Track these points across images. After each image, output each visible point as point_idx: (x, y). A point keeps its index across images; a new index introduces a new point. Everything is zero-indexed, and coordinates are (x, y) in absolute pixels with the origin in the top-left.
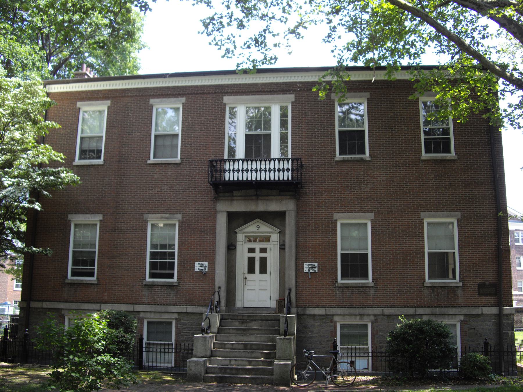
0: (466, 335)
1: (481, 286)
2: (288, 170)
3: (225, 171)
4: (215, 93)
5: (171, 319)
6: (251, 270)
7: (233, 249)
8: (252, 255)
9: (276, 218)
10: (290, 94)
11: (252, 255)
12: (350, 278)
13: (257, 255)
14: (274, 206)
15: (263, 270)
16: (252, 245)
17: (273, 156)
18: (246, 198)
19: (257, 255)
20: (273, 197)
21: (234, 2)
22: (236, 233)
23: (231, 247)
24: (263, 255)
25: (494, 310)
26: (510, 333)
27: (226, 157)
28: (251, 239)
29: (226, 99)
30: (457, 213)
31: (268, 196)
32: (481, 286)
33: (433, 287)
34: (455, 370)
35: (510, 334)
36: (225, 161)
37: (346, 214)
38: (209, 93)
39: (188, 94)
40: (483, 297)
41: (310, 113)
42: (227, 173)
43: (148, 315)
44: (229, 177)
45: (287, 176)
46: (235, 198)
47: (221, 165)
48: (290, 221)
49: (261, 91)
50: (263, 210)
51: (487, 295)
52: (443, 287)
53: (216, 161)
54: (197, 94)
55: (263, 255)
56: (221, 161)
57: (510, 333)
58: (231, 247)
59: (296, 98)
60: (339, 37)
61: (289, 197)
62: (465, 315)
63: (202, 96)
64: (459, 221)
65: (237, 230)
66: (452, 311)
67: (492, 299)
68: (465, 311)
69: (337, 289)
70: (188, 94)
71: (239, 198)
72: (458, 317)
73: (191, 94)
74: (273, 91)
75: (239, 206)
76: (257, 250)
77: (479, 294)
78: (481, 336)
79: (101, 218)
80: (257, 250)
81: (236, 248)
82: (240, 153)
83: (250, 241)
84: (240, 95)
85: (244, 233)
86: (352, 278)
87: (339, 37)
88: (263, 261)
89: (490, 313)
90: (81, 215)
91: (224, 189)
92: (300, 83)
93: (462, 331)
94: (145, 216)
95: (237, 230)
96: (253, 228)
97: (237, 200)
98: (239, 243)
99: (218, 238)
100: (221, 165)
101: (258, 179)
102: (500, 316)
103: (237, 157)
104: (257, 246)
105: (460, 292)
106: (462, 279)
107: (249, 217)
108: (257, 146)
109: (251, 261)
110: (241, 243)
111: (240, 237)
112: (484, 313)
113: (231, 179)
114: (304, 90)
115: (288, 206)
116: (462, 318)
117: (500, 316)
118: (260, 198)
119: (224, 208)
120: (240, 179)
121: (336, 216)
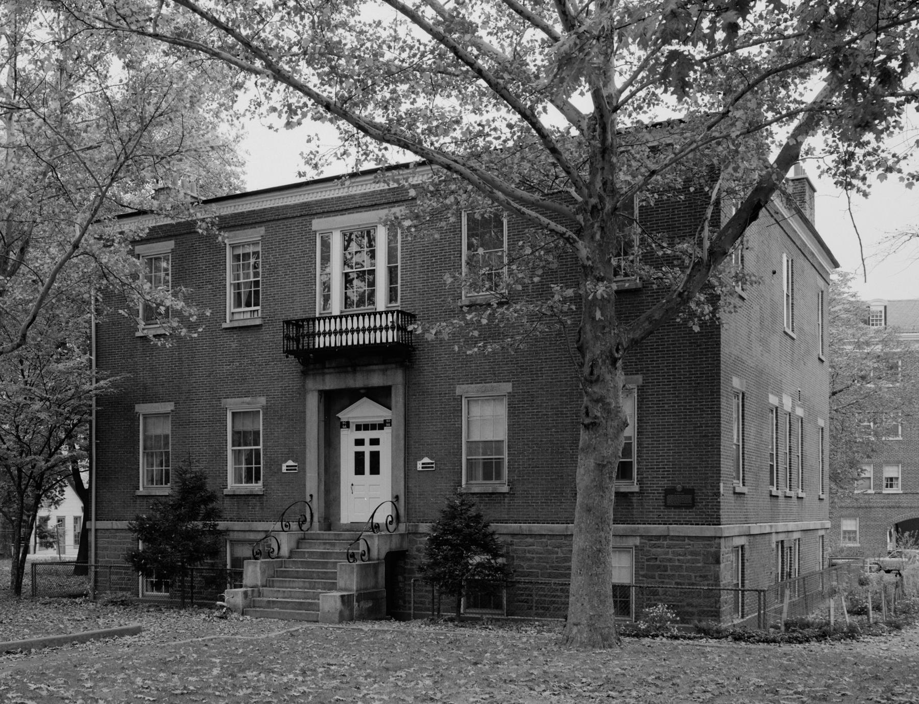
1: (669, 491)
2: (319, 334)
4: (301, 216)
6: (359, 470)
8: (360, 449)
9: (381, 396)
11: (360, 449)
13: (367, 449)
14: (376, 380)
15: (375, 470)
16: (361, 435)
18: (342, 370)
19: (367, 449)
20: (375, 367)
21: (1, 298)
24: (375, 448)
29: (318, 224)
30: (636, 376)
31: (366, 365)
37: (473, 386)
38: (293, 217)
44: (321, 342)
45: (391, 336)
46: (326, 371)
48: (398, 398)
50: (381, 385)
53: (303, 320)
54: (278, 220)
55: (375, 448)
56: (308, 320)
61: (394, 366)
63: (285, 221)
71: (331, 370)
75: (331, 383)
76: (367, 442)
77: (667, 506)
80: (367, 442)
82: (336, 307)
88: (375, 456)
91: (314, 360)
94: (223, 401)
97: (330, 373)
99: (308, 427)
101: (355, 343)
103: (333, 314)
104: (367, 435)
107: (352, 396)
109: (359, 457)
113: (367, 342)
115: (396, 379)
116: (637, 541)
118: (358, 368)
119: (315, 385)
120: (327, 344)
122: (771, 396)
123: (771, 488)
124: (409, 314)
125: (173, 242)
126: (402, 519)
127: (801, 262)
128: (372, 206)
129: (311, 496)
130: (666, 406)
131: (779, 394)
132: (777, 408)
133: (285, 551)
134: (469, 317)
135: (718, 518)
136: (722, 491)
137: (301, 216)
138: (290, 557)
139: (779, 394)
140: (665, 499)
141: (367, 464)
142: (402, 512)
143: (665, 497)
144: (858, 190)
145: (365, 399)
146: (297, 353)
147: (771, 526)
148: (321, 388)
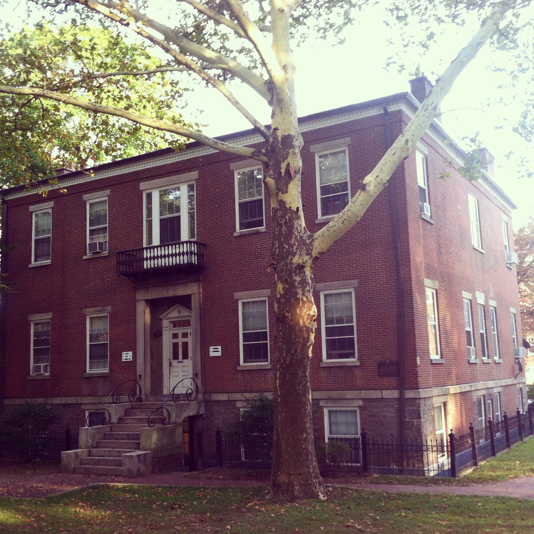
0: (366, 424)
1: (381, 365)
3: (143, 259)
4: (133, 181)
5: (103, 409)
6: (175, 356)
7: (159, 336)
8: (176, 341)
10: (194, 171)
11: (176, 341)
12: (253, 360)
13: (180, 340)
15: (185, 356)
17: (182, 240)
22: (161, 320)
23: (156, 334)
25: (394, 394)
26: (415, 422)
27: (145, 246)
28: (175, 324)
29: (143, 186)
30: (353, 281)
32: (381, 365)
33: (329, 368)
34: (358, 465)
35: (415, 423)
36: (143, 249)
38: (128, 182)
39: (111, 185)
40: (385, 378)
41: (212, 189)
42: (145, 262)
43: (88, 407)
44: (147, 265)
47: (140, 254)
49: (169, 173)
51: (388, 376)
52: (341, 367)
53: (136, 250)
54: (118, 184)
57: (415, 422)
58: (157, 334)
59: (199, 175)
60: (444, 63)
62: (364, 400)
64: (356, 289)
65: (161, 317)
66: (349, 394)
67: (393, 380)
68: (364, 394)
69: (238, 372)
70: (111, 185)
72: (356, 401)
73: (114, 185)
74: (179, 170)
76: (180, 335)
77: (380, 375)
78: (383, 425)
79: (52, 316)
80: (180, 335)
81: (162, 334)
83: (175, 326)
84: (153, 179)
85: (168, 319)
86: (255, 360)
87: (444, 63)
88: (185, 345)
89: (391, 397)
90: (37, 315)
92: (202, 157)
93: (362, 419)
95: (161, 317)
96: (175, 313)
98: (164, 329)
100: (140, 254)
102: (401, 401)
104: (180, 331)
105: (358, 373)
106: (360, 359)
108: (170, 229)
109: (175, 345)
110: (166, 329)
111: (165, 323)
112: (384, 397)
114: (205, 164)
115: (193, 290)
116: (361, 403)
117: (401, 401)
119: (142, 296)
121: (237, 295)
122: (463, 292)
123: (483, 358)
124: (202, 244)
125: (53, 202)
126: (200, 391)
127: (486, 202)
128: (177, 171)
129: (140, 376)
130: (375, 302)
131: (472, 290)
132: (471, 301)
133: (114, 419)
134: (287, 247)
135: (417, 383)
136: (418, 363)
137: (133, 181)
138: (118, 423)
139: (472, 290)
140: (379, 371)
141: (180, 352)
142: (200, 385)
143: (378, 368)
144: (137, 55)
145: (177, 305)
146: (128, 275)
147: (471, 386)
148: (146, 298)
